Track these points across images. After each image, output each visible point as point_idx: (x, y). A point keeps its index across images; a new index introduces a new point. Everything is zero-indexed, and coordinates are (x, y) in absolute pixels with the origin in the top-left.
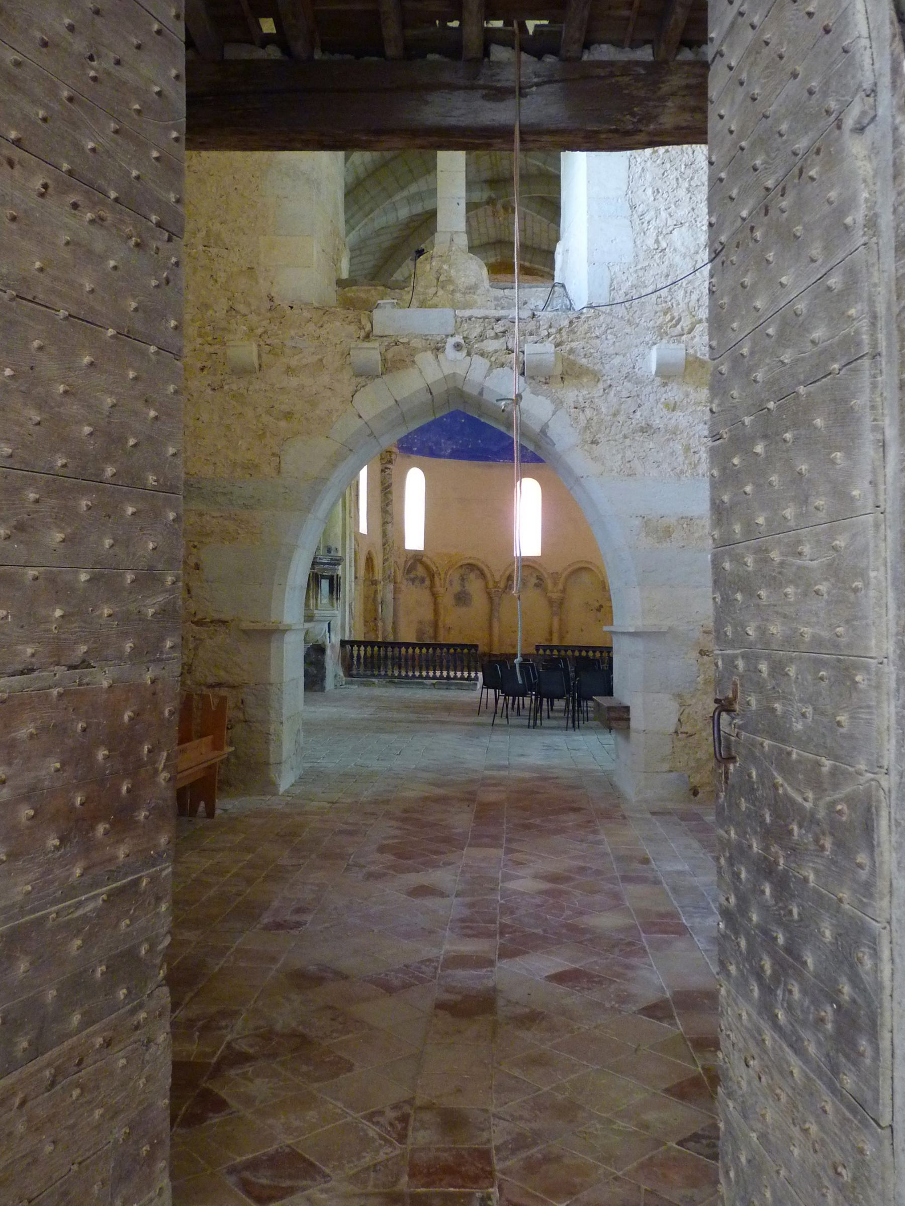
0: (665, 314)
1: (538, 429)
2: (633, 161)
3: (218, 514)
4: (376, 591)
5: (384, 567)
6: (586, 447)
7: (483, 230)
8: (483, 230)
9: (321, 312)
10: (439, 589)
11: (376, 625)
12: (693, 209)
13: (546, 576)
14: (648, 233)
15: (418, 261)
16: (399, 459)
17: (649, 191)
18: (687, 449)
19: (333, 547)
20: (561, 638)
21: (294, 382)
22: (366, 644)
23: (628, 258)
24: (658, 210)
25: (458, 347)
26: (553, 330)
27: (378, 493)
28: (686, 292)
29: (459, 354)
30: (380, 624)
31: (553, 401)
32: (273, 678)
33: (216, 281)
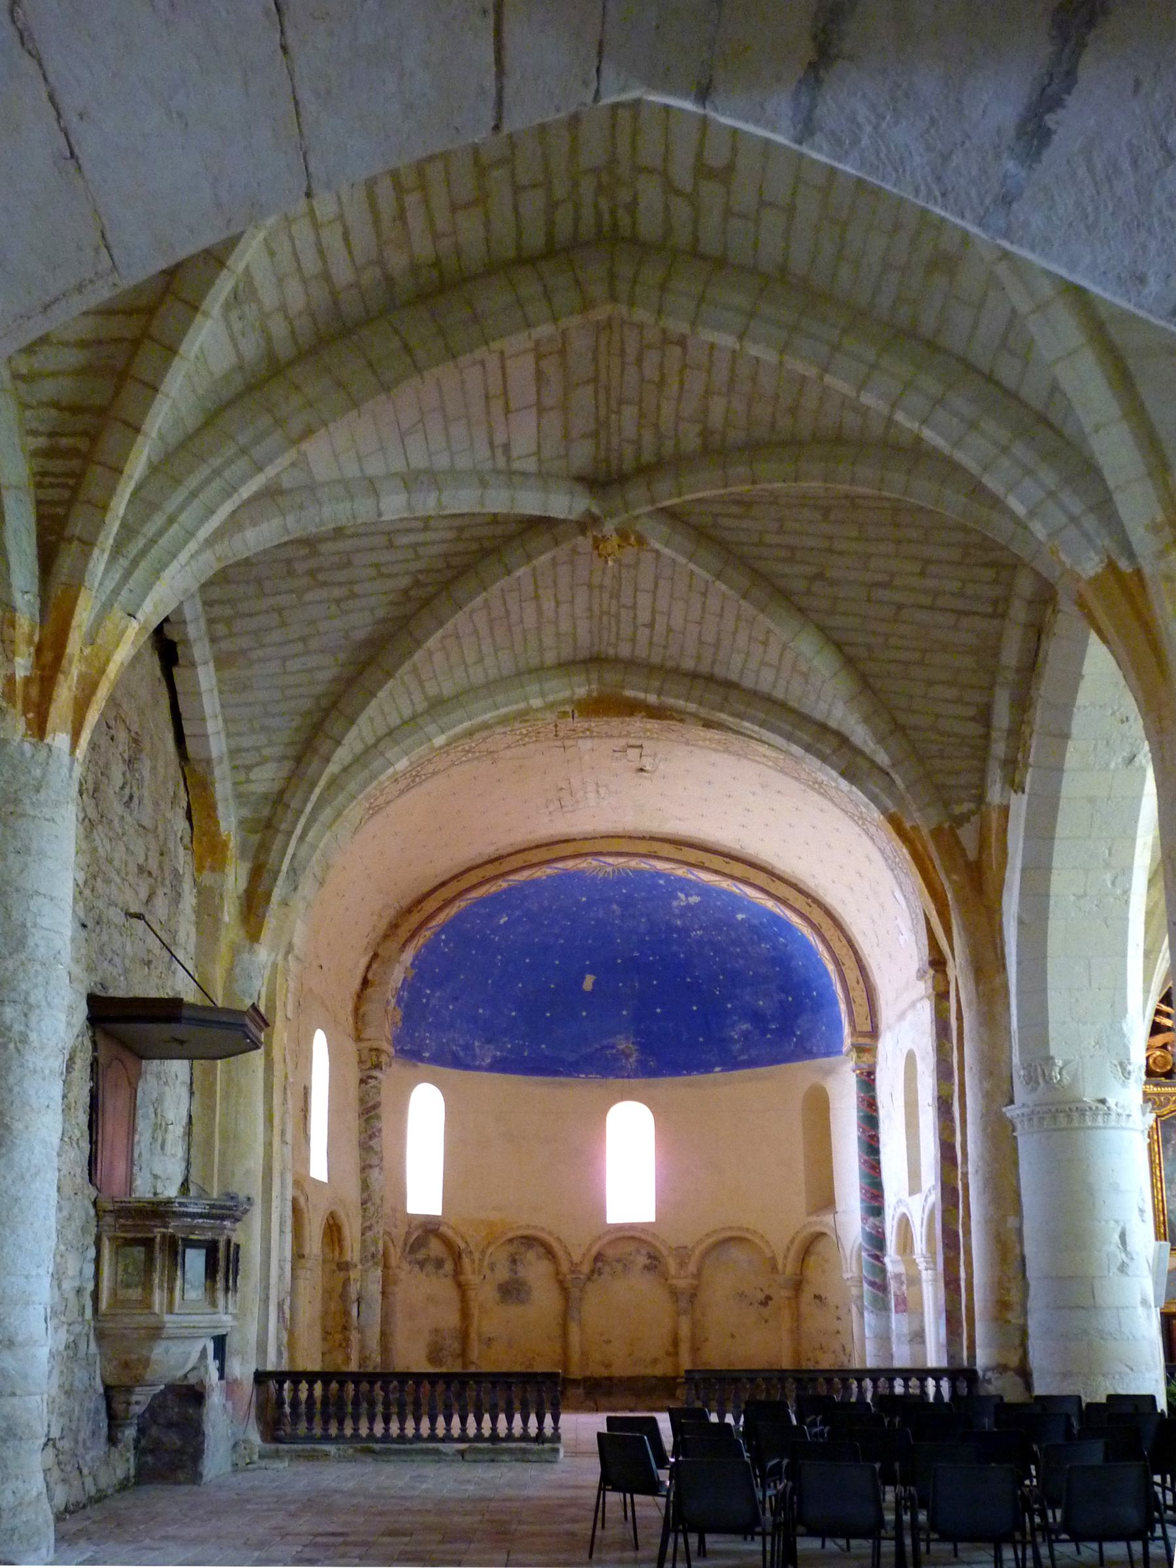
4: (346, 1282)
5: (363, 1242)
7: (565, 626)
8: (565, 626)
10: (470, 1275)
13: (665, 1252)
19: (242, 1197)
20: (695, 1350)
22: (325, 1377)
27: (352, 1120)
30: (354, 1336)
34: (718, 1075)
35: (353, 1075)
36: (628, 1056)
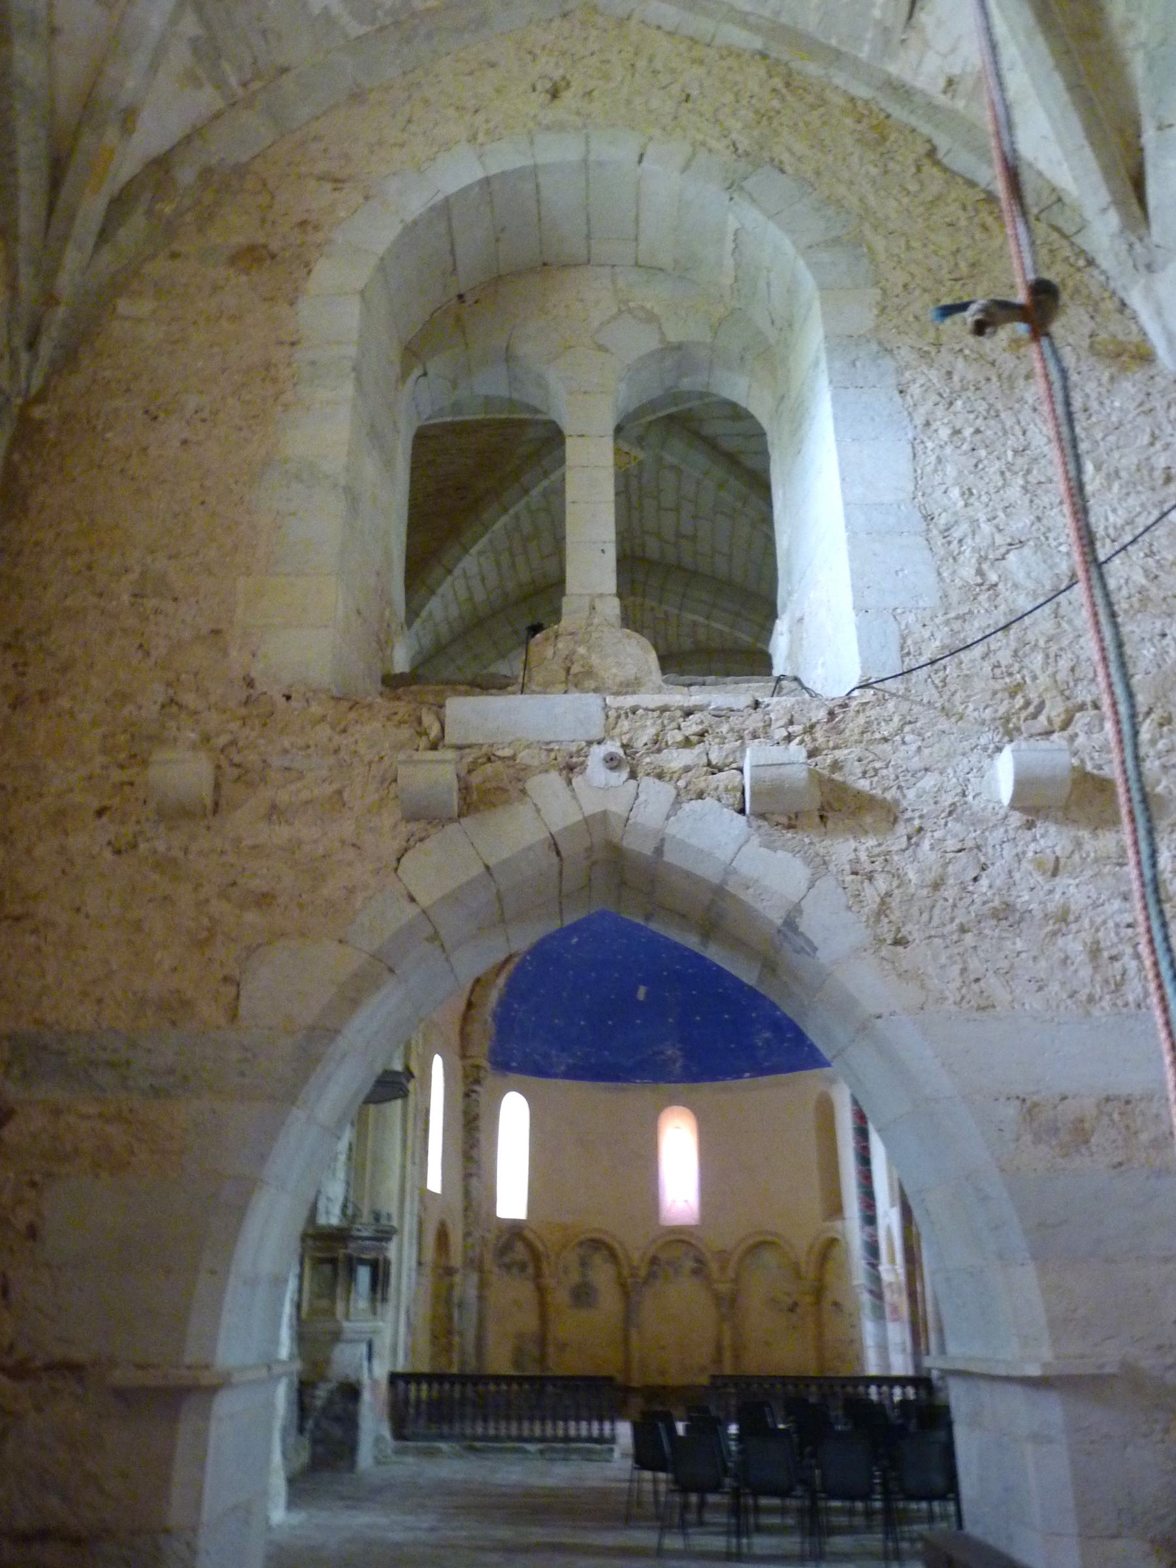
0: (1013, 695)
1: (777, 918)
2: (919, 448)
3: (92, 1110)
4: (451, 1287)
6: (884, 953)
9: (345, 705)
10: (549, 1282)
11: (450, 1344)
12: (1039, 519)
13: (708, 1255)
14: (961, 558)
15: (533, 641)
16: (491, 1080)
17: (955, 493)
18: (1095, 952)
19: (384, 1213)
20: (737, 1358)
21: (282, 833)
22: (429, 1378)
23: (930, 600)
24: (974, 522)
25: (612, 762)
26: (796, 729)
27: (459, 1133)
28: (1047, 656)
29: (615, 774)
30: (456, 1339)
31: (808, 861)
32: (176, 1516)
33: (148, 654)
34: (746, 1081)
35: (460, 1089)
36: (674, 1062)
